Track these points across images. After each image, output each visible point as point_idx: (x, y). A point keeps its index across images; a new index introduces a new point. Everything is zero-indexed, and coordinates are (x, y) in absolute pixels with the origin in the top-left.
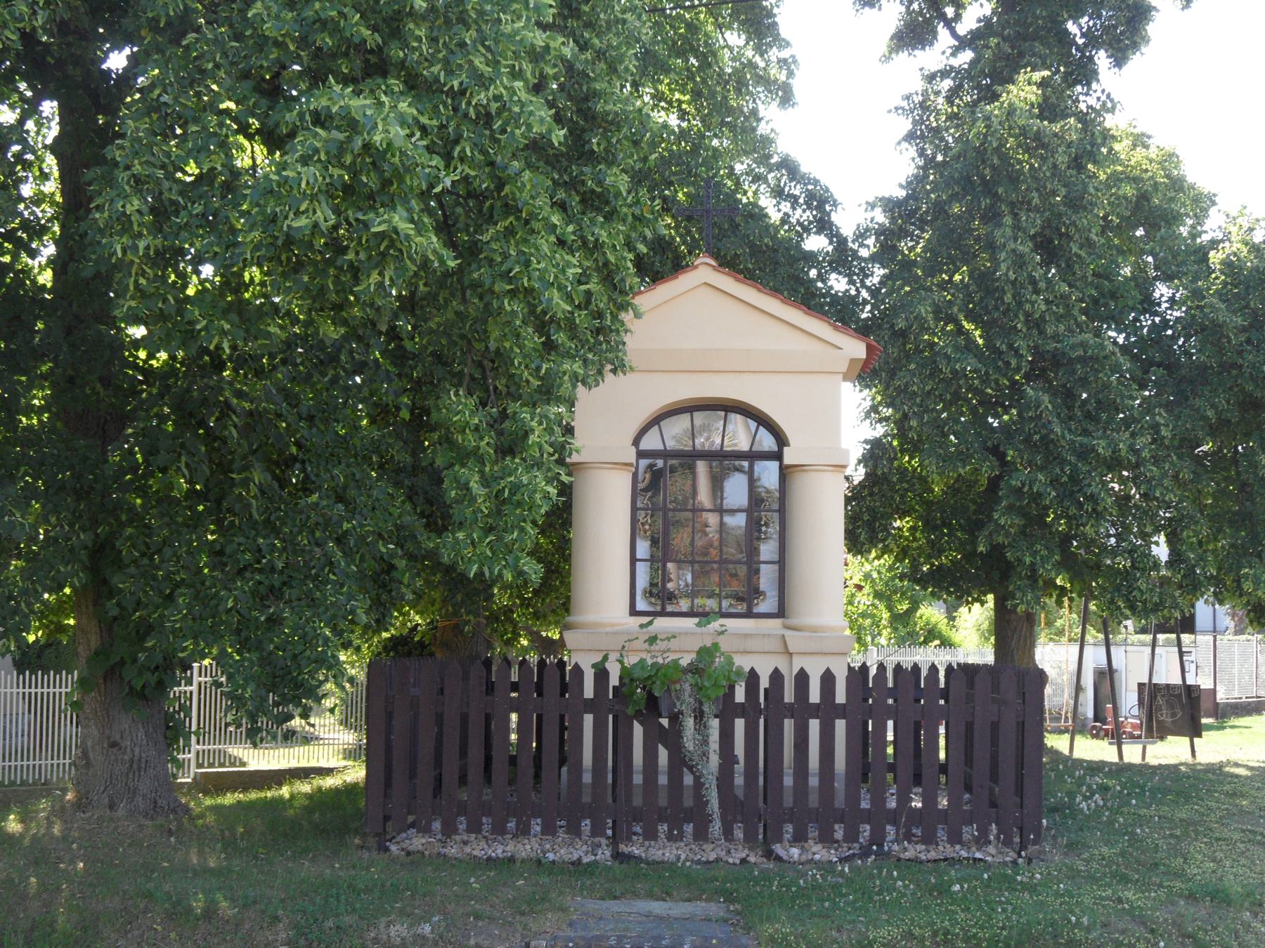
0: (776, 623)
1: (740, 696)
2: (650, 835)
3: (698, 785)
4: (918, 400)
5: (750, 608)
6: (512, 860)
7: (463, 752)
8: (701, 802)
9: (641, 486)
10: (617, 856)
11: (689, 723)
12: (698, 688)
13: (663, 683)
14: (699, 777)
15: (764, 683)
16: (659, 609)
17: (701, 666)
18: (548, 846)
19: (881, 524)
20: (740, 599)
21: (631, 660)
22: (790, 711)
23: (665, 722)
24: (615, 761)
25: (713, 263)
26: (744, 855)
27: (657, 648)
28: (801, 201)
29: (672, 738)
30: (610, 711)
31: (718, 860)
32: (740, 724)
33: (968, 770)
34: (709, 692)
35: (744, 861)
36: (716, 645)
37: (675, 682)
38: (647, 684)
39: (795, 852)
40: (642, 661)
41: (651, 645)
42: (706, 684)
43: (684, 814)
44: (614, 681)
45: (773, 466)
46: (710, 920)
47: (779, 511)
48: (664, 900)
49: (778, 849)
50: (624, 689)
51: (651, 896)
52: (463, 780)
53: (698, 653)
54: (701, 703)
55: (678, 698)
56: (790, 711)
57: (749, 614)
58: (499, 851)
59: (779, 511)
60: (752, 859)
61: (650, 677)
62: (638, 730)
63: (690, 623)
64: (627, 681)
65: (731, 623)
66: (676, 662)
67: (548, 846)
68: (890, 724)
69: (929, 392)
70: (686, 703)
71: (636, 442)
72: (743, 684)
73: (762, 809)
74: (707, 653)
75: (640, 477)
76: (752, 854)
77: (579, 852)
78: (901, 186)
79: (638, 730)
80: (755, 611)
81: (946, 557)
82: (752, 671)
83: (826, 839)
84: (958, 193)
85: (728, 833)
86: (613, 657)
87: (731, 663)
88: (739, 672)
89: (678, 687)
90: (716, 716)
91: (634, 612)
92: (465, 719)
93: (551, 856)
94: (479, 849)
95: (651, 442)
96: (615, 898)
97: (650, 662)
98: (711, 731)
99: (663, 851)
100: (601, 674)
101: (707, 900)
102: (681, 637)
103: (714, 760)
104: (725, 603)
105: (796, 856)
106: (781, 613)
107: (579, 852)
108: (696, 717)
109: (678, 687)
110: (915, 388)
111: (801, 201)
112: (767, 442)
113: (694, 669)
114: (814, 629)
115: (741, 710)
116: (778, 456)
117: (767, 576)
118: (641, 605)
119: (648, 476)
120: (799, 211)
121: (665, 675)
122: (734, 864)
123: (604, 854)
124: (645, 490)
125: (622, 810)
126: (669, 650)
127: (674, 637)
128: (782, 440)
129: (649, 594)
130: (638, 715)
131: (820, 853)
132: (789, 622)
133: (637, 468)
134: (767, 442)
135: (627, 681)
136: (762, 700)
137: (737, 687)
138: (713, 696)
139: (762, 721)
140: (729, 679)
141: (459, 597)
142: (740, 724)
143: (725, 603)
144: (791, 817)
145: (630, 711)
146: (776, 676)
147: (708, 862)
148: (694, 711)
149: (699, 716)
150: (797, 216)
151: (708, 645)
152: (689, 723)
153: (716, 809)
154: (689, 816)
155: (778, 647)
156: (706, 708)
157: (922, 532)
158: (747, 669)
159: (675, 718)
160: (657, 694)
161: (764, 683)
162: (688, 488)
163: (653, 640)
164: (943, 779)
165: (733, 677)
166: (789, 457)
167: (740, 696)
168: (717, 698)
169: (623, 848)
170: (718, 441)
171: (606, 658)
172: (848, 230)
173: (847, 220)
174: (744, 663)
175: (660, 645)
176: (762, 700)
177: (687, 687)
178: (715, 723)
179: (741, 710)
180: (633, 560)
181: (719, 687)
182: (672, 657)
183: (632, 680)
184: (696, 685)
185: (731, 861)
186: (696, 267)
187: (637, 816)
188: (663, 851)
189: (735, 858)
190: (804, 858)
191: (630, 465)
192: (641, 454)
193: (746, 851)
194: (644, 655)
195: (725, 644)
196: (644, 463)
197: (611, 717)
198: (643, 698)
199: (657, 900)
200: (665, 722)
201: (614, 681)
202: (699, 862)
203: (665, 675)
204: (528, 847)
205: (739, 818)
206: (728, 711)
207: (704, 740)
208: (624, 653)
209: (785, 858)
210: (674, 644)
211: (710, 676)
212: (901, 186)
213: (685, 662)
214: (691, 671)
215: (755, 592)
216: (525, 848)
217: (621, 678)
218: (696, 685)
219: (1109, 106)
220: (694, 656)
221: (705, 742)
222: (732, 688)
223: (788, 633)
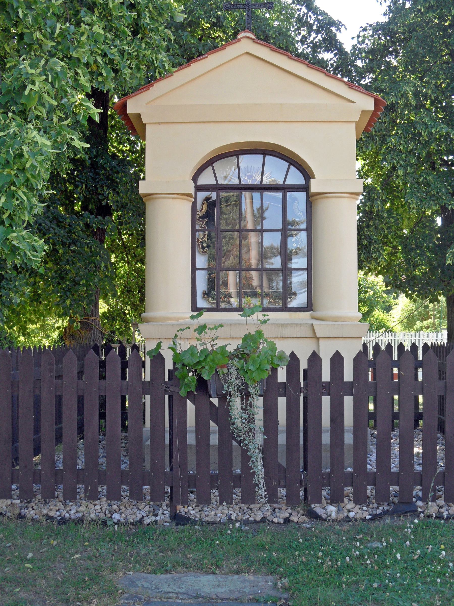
0: (306, 315)
1: (282, 376)
2: (204, 500)
3: (246, 457)
4: (403, 156)
5: (285, 303)
6: (81, 520)
7: (59, 419)
8: (248, 472)
9: (199, 214)
10: (177, 518)
11: (237, 402)
12: (243, 371)
13: (211, 367)
14: (247, 451)
15: (303, 365)
16: (214, 306)
17: (246, 352)
18: (115, 507)
19: (375, 247)
20: (277, 298)
21: (184, 346)
22: (327, 389)
23: (215, 401)
24: (171, 440)
25: (253, 37)
26: (287, 515)
27: (207, 336)
28: (315, 28)
29: (222, 415)
30: (166, 392)
31: (264, 520)
32: (282, 401)
33: (442, 417)
34: (254, 375)
35: (287, 520)
36: (259, 333)
37: (222, 367)
38: (196, 367)
39: (332, 509)
40: (192, 348)
41: (200, 333)
42: (251, 368)
43: (232, 482)
44: (169, 365)
45: (302, 196)
46: (258, 601)
47: (306, 230)
48: (214, 573)
49: (318, 509)
50: (176, 373)
51: (202, 569)
52: (59, 439)
53: (244, 340)
54: (247, 385)
55: (226, 381)
56: (327, 389)
57: (285, 309)
58: (72, 512)
59: (306, 230)
60: (294, 518)
61: (199, 363)
62: (191, 407)
63: (236, 316)
64: (179, 366)
65: (272, 316)
66: (223, 348)
67: (115, 507)
68: (370, 380)
69: (412, 150)
70: (233, 386)
71: (195, 178)
72: (285, 367)
73: (303, 473)
74: (251, 340)
75: (199, 207)
76: (294, 513)
77: (141, 512)
78: (385, 14)
79: (191, 407)
80: (289, 306)
81: (419, 270)
82: (293, 355)
83: (360, 499)
84: (433, 6)
85: (272, 497)
86: (165, 345)
87: (273, 348)
88: (281, 357)
89: (225, 371)
90: (260, 396)
91: (194, 308)
92: (37, 401)
93: (116, 516)
94: (56, 509)
95: (206, 179)
96: (166, 572)
97: (199, 348)
98: (256, 410)
99: (217, 513)
100: (158, 359)
101: (256, 573)
102: (229, 329)
103: (260, 439)
104: (266, 301)
105: (334, 515)
106: (309, 307)
107: (141, 512)
108: (242, 398)
109: (225, 371)
110: (401, 147)
111: (315, 28)
112: (295, 178)
113: (240, 354)
114: (336, 319)
115: (283, 389)
116: (305, 188)
117: (298, 279)
118: (201, 303)
119: (205, 206)
120: (313, 35)
121: (213, 361)
122: (278, 523)
123: (164, 515)
124: (203, 217)
125: (177, 477)
126: (217, 338)
127: (221, 326)
128: (307, 174)
129: (207, 294)
130: (190, 395)
131: (356, 511)
132: (315, 314)
133: (196, 199)
134: (295, 178)
135: (179, 366)
136: (301, 380)
137: (279, 370)
138: (258, 379)
139: (301, 398)
140: (272, 363)
141: (68, 302)
142: (282, 401)
143: (266, 301)
144: (329, 480)
145: (183, 393)
146: (315, 359)
147: (255, 522)
148: (241, 392)
149: (245, 396)
150: (311, 38)
151: (253, 332)
152: (237, 402)
153: (262, 480)
154: (238, 481)
155: (310, 334)
156: (251, 390)
157: (402, 253)
158: (288, 354)
159: (224, 398)
160: (205, 378)
161: (303, 365)
162: (236, 217)
163: (202, 328)
164: (396, 408)
165: (276, 361)
166: (314, 187)
167: (282, 376)
168: (262, 380)
169: (181, 509)
170: (259, 179)
171: (159, 346)
172: (348, 48)
173: (347, 39)
174: (285, 347)
175: (209, 333)
176: (301, 380)
177: (233, 370)
178: (259, 402)
179: (283, 389)
180: (194, 269)
181: (263, 370)
182: (221, 343)
183: (183, 365)
184: (242, 369)
185: (276, 520)
186: (240, 40)
187: (192, 482)
188: (217, 513)
189: (279, 518)
190: (341, 516)
191: (189, 195)
192: (199, 189)
193: (289, 511)
194: (194, 343)
195: (267, 332)
196: (202, 195)
197: (167, 397)
198: (199, 380)
199: (207, 573)
200: (215, 401)
201: (169, 365)
202: (246, 523)
203: (213, 361)
204: (98, 507)
205: (282, 483)
206: (271, 390)
207: (249, 416)
208: (178, 341)
209: (324, 516)
210: (220, 332)
211: (254, 361)
212: (385, 14)
213: (231, 349)
214: (237, 356)
215: (289, 291)
216: (94, 510)
217: (174, 364)
218: (242, 369)
219: (362, 175)
220: (240, 342)
221: (251, 420)
222: (274, 370)
223: (315, 322)
